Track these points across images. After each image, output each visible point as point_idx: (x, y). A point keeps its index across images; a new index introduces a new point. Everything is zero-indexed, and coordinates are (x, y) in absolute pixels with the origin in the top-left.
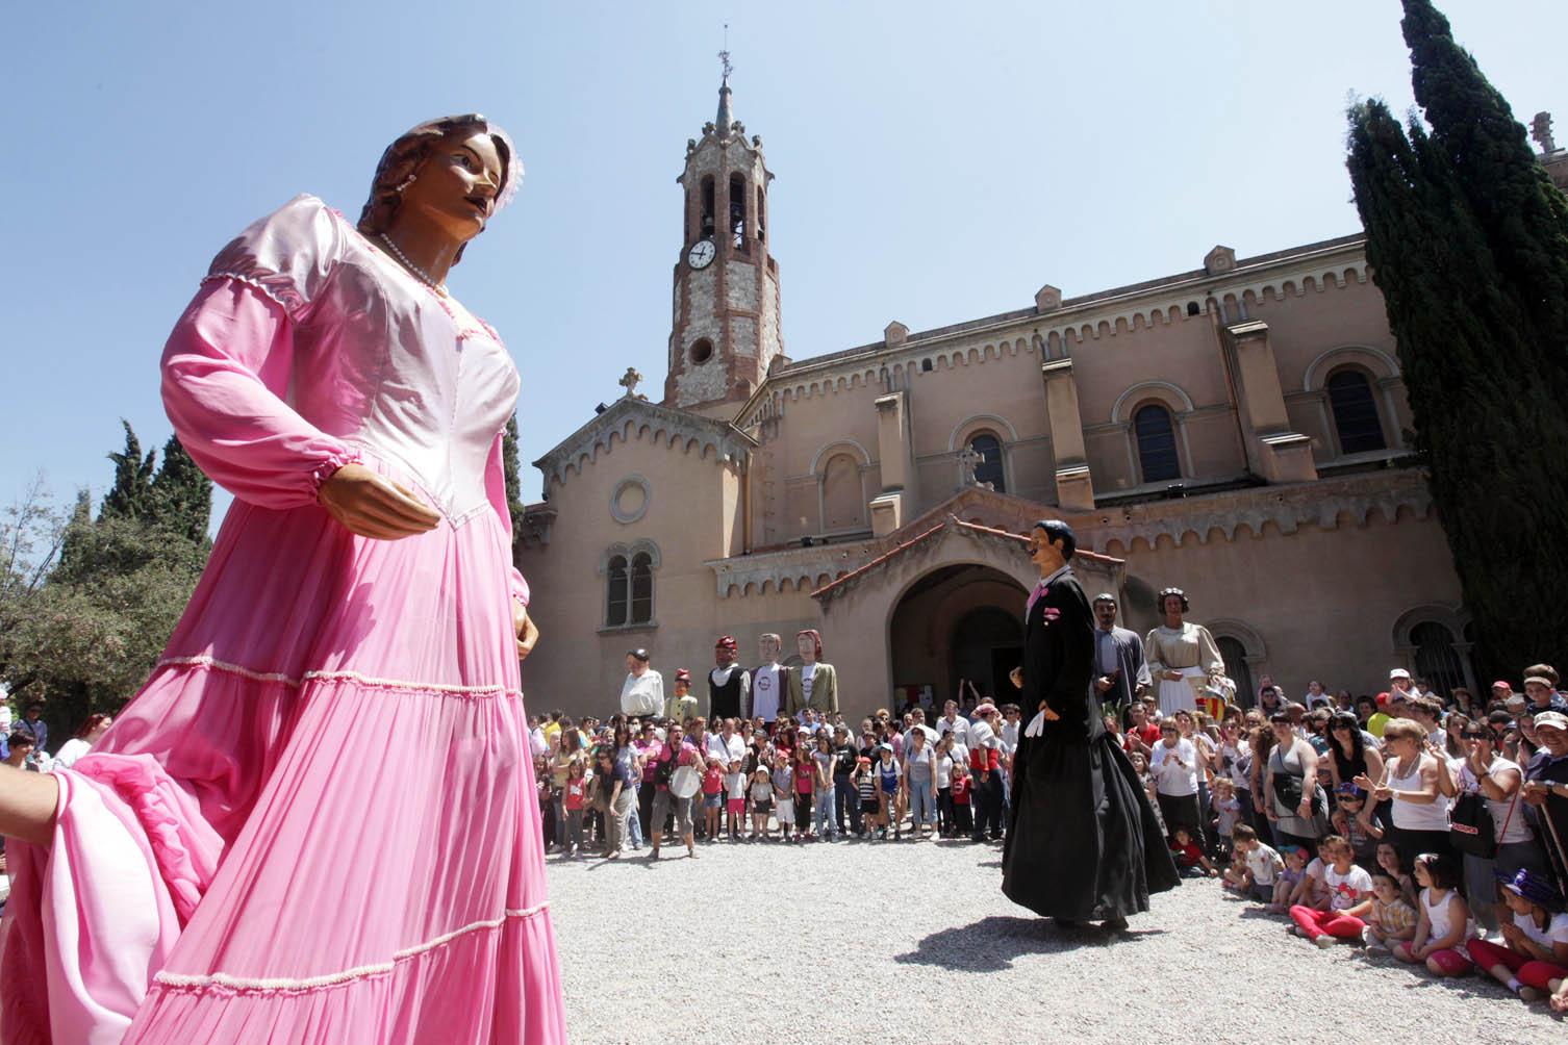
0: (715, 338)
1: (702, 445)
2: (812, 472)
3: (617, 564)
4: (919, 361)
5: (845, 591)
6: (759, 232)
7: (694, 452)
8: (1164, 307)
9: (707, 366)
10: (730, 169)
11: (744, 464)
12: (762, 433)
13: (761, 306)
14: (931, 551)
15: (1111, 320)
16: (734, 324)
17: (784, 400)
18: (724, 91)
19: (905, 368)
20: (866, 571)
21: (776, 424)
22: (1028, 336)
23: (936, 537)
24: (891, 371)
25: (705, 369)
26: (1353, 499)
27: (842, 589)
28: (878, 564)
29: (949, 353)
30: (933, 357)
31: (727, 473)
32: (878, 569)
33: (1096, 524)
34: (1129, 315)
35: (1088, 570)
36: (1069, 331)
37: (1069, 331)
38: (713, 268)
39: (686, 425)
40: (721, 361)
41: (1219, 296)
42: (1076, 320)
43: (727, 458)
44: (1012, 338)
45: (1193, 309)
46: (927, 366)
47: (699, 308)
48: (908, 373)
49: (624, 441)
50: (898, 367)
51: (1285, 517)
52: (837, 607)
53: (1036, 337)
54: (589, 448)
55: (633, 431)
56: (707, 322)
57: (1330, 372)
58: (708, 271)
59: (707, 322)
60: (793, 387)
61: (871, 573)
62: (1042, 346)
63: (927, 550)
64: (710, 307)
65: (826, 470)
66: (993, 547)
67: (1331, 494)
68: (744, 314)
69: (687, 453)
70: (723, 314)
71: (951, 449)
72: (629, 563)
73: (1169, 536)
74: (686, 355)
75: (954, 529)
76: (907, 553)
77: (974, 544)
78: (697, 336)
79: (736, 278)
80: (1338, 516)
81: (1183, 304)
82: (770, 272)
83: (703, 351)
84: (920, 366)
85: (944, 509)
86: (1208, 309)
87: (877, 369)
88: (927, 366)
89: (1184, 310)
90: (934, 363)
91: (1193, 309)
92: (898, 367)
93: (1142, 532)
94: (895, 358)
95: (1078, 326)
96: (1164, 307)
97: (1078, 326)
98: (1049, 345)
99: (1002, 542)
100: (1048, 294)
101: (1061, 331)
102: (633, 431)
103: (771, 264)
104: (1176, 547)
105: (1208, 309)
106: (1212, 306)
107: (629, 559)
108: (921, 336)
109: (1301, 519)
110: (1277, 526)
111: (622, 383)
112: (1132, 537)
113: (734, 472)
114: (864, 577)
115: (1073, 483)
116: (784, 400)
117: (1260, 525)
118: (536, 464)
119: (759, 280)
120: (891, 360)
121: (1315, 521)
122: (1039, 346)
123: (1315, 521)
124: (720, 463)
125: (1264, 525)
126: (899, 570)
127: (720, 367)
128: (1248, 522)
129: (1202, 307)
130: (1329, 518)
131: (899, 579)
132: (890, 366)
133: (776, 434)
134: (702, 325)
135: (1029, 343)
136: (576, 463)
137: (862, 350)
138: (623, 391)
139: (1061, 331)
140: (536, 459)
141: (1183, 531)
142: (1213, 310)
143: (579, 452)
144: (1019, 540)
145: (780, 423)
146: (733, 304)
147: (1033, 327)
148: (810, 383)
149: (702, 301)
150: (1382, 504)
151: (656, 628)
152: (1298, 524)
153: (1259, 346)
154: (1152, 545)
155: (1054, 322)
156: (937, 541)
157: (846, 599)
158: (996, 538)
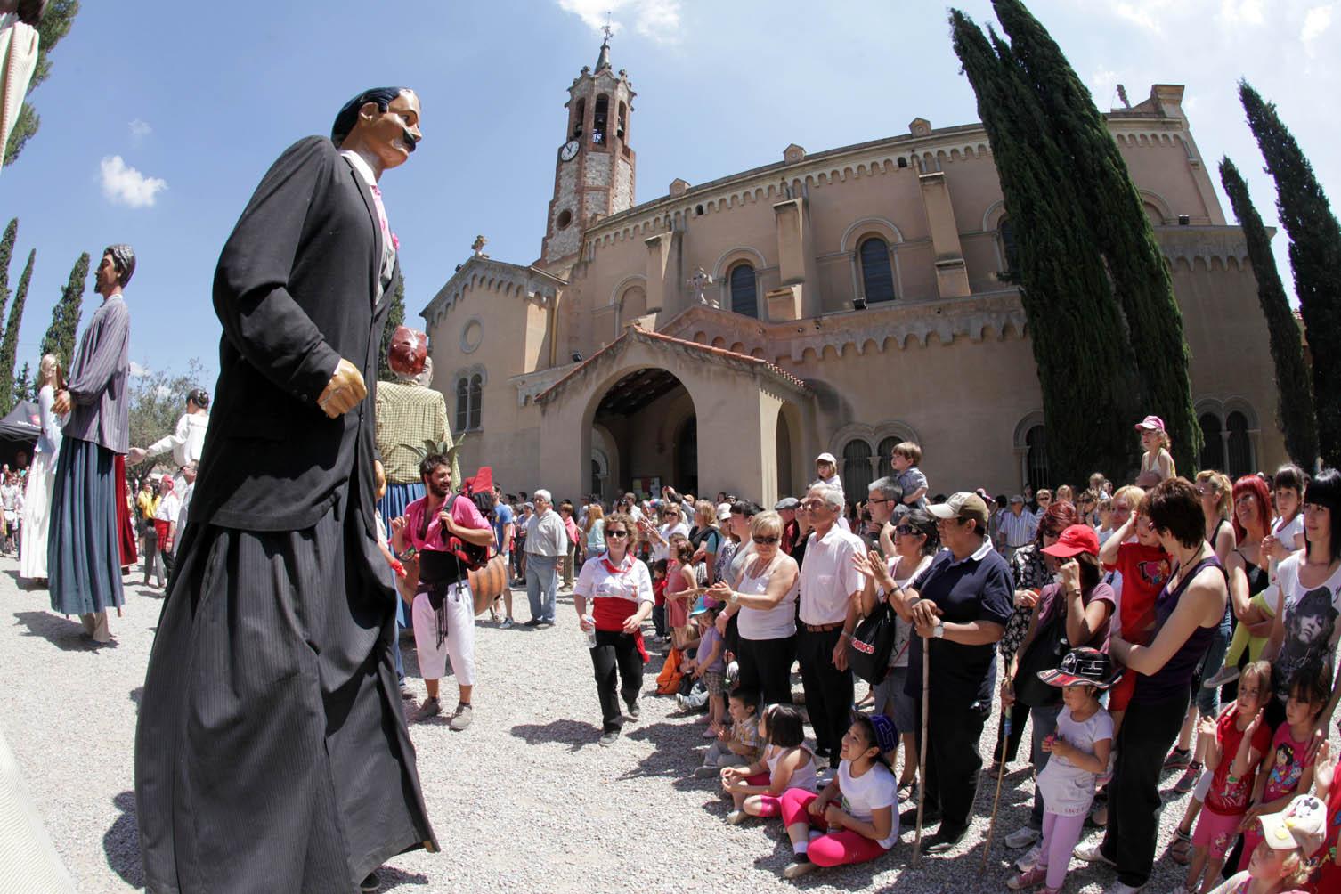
0: (574, 209)
1: (515, 287)
2: (611, 303)
3: (463, 382)
4: (693, 207)
5: (557, 395)
6: (619, 131)
7: (513, 292)
8: (880, 160)
10: (598, 91)
11: (551, 300)
12: (572, 276)
13: (613, 182)
14: (618, 357)
15: (841, 169)
17: (595, 247)
18: (603, 48)
19: (683, 213)
20: (570, 377)
21: (586, 267)
22: (777, 183)
23: (620, 345)
24: (672, 217)
25: (566, 232)
26: (994, 315)
27: (554, 394)
28: (578, 371)
29: (716, 200)
30: (704, 204)
31: (533, 308)
32: (579, 376)
33: (795, 334)
34: (854, 166)
35: (736, 370)
36: (809, 178)
37: (809, 178)
38: (577, 159)
39: (507, 273)
40: (577, 225)
41: (920, 153)
42: (815, 169)
43: (532, 294)
44: (764, 185)
45: (902, 163)
46: (700, 211)
47: (565, 189)
48: (685, 217)
49: (471, 291)
50: (677, 213)
51: (944, 329)
52: (551, 409)
54: (451, 299)
55: (477, 282)
56: (570, 197)
57: (1000, 220)
59: (570, 197)
60: (602, 237)
61: (573, 379)
62: (788, 190)
63: (615, 356)
64: (573, 186)
65: (622, 301)
66: (664, 351)
67: (978, 310)
68: (597, 189)
69: (497, 292)
70: (581, 190)
72: (469, 383)
73: (853, 344)
74: (555, 223)
75: (635, 337)
76: (600, 360)
77: (650, 350)
78: (562, 208)
79: (594, 164)
80: (983, 329)
81: (894, 158)
83: (565, 219)
84: (694, 211)
85: (674, 323)
86: (913, 163)
87: (662, 216)
88: (700, 211)
89: (895, 163)
90: (705, 208)
91: (902, 163)
92: (677, 213)
93: (831, 341)
94: (676, 207)
95: (815, 174)
96: (880, 160)
97: (815, 174)
98: (793, 190)
99: (669, 346)
100: (793, 151)
101: (802, 179)
102: (477, 282)
103: (627, 152)
104: (859, 355)
105: (913, 163)
106: (915, 160)
107: (469, 379)
108: (697, 188)
109: (956, 331)
110: (939, 336)
111: (474, 247)
112: (824, 345)
113: (541, 306)
114: (569, 382)
115: (780, 298)
116: (595, 247)
117: (924, 336)
118: (421, 315)
119: (612, 164)
120: (672, 208)
121: (966, 334)
122: (785, 190)
123: (966, 334)
124: (528, 300)
125: (928, 336)
126: (594, 375)
127: (576, 229)
128: (915, 333)
129: (908, 161)
130: (976, 332)
131: (594, 382)
132: (672, 214)
133: (586, 275)
134: (568, 201)
135: (778, 188)
136: (444, 311)
137: (653, 203)
138: (473, 253)
139: (802, 179)
140: (421, 311)
141: (865, 339)
142: (916, 164)
143: (445, 303)
144: (682, 344)
145: (590, 266)
146: (589, 182)
147: (780, 176)
148: (614, 232)
149: (569, 183)
150: (1015, 321)
151: (482, 432)
152: (954, 336)
153: (939, 188)
154: (839, 353)
155: (797, 171)
156: (622, 349)
157: (557, 403)
158: (665, 344)
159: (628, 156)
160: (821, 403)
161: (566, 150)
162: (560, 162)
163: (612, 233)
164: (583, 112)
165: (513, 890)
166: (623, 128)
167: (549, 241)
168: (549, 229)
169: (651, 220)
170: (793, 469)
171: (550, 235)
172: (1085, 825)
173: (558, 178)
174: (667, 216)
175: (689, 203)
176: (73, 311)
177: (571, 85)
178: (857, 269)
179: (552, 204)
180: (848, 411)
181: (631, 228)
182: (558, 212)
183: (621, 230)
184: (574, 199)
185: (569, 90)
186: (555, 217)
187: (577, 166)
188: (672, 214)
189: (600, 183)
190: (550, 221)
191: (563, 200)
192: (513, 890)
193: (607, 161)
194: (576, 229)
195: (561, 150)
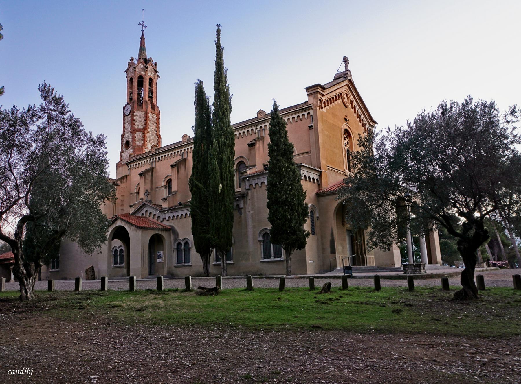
0: (130, 140)
4: (157, 157)
9: (129, 150)
16: (136, 135)
38: (130, 115)
40: (132, 149)
53: (181, 151)
58: (129, 116)
60: (132, 165)
64: (130, 129)
71: (163, 185)
74: (124, 146)
79: (138, 117)
82: (153, 111)
84: (157, 159)
87: (149, 160)
90: (160, 158)
127: (132, 150)
132: (151, 159)
133: (127, 180)
145: (128, 177)
159: (155, 110)
160: (172, 233)
161: (126, 109)
162: (124, 115)
163: (135, 164)
164: (141, 46)
165: (146, 381)
166: (152, 94)
167: (122, 154)
168: (122, 148)
169: (146, 161)
170: (431, 249)
171: (122, 152)
172: (250, 290)
173: (124, 123)
174: (150, 160)
175: (156, 156)
176: (163, 230)
177: (126, 68)
178: (166, 192)
179: (123, 136)
180: (178, 235)
181: (140, 163)
182: (125, 141)
183: (137, 163)
184: (130, 135)
185: (126, 71)
186: (124, 143)
187: (130, 119)
188: (151, 159)
189: (141, 127)
190: (122, 144)
191: (127, 135)
192: (146, 381)
193: (143, 116)
194: (132, 150)
195: (124, 108)
